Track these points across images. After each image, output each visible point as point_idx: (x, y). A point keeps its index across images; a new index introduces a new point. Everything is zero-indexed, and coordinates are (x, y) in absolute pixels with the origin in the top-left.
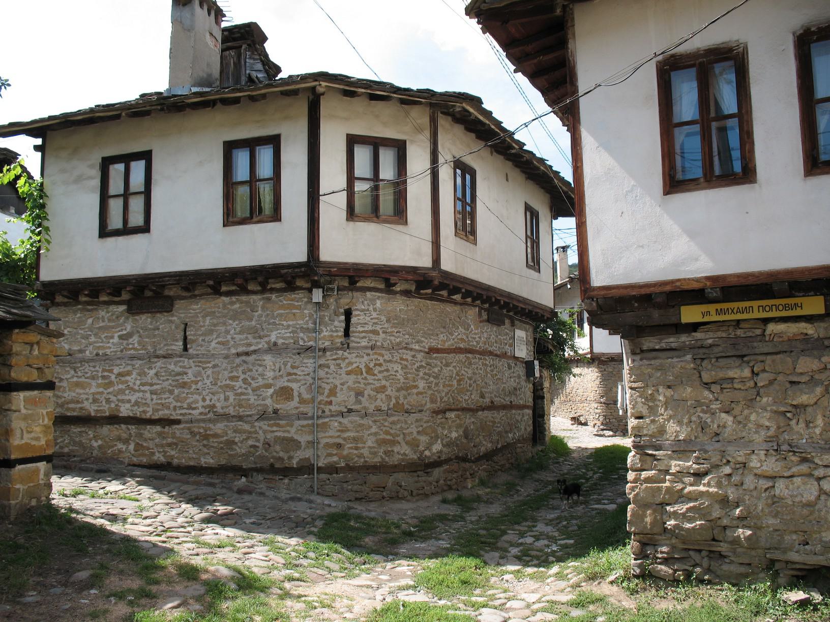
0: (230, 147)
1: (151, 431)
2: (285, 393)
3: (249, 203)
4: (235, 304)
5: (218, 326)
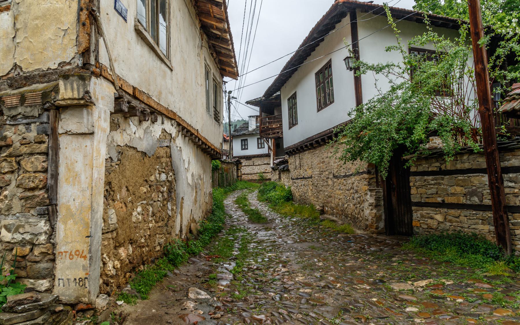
0: (242, 140)
1: (249, 175)
2: (266, 170)
3: (244, 146)
4: (260, 158)
5: (257, 161)
